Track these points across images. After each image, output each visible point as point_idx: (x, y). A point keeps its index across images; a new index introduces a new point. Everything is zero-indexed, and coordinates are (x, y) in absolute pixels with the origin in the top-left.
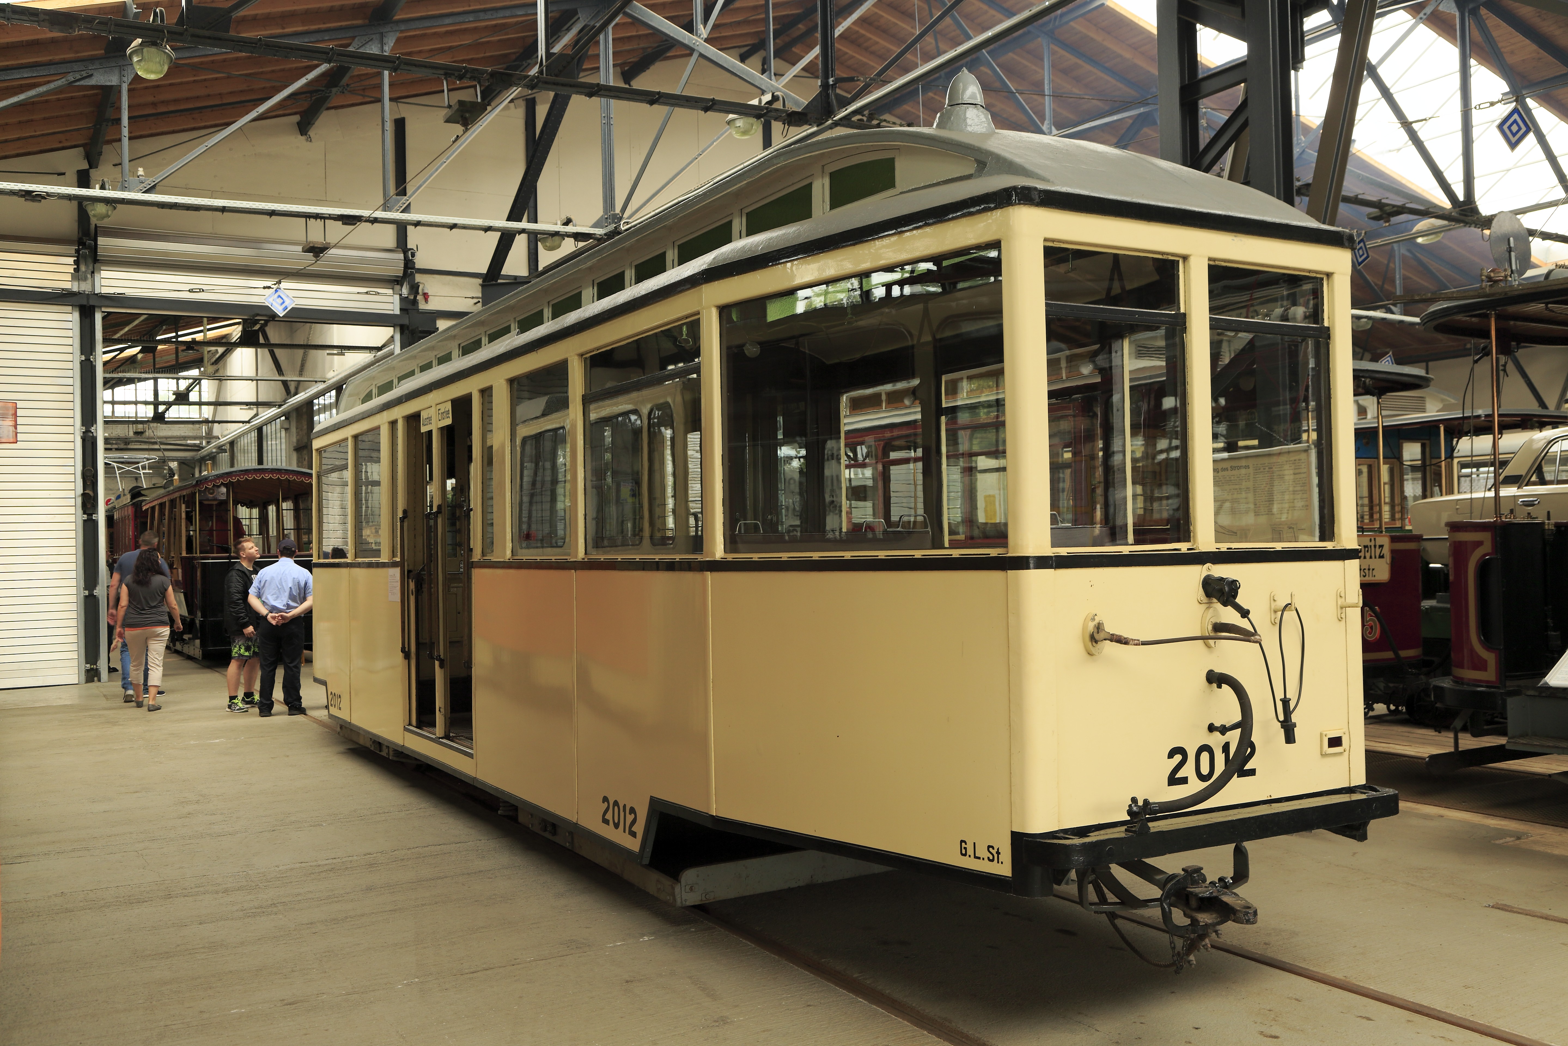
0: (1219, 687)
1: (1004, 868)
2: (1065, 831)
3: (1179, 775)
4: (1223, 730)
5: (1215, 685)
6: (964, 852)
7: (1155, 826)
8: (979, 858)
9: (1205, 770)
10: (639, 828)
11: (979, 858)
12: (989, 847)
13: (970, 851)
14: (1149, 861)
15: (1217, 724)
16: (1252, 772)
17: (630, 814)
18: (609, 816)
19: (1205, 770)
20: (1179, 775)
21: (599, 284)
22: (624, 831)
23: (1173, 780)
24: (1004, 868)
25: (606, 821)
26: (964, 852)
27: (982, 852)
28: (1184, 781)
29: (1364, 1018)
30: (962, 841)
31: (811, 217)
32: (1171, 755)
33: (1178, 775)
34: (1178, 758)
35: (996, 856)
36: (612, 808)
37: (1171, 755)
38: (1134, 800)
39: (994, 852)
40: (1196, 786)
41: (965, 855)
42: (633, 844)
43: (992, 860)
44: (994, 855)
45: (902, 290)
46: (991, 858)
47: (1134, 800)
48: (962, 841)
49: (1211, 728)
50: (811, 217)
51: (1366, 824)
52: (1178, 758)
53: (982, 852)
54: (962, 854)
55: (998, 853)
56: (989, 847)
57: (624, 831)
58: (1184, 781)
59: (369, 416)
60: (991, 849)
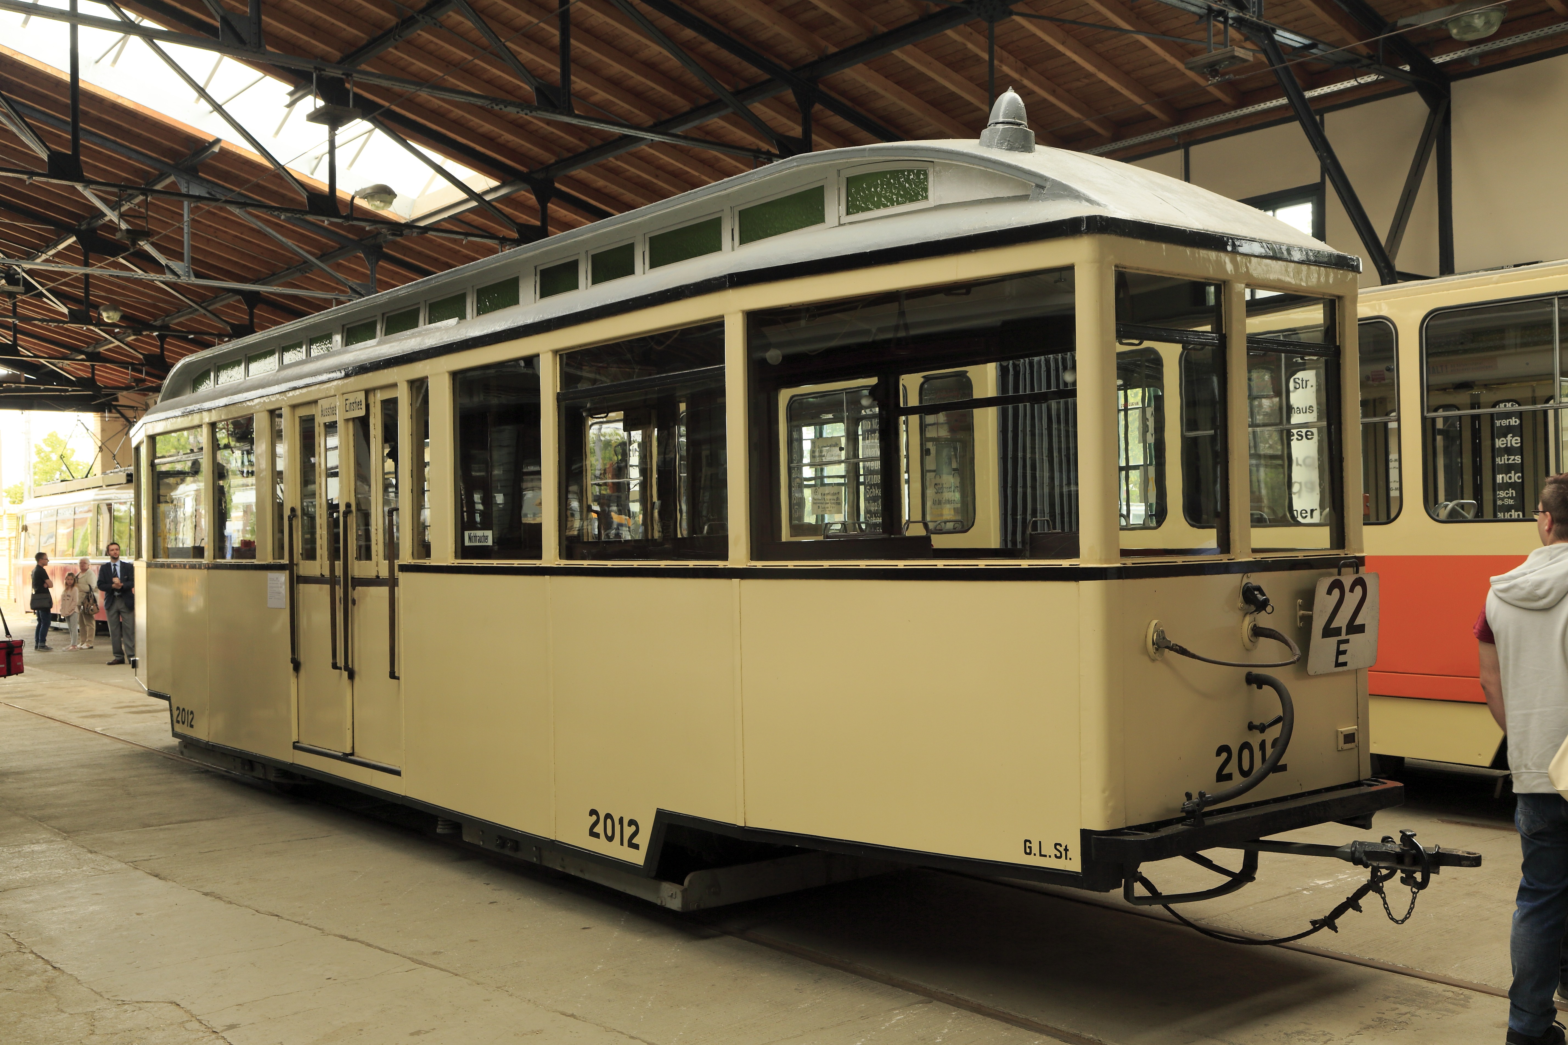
0: (1260, 687)
1: (1074, 864)
2: (1129, 828)
3: (1225, 772)
4: (1262, 728)
5: (1255, 686)
6: (1028, 850)
7: (1209, 821)
8: (1045, 856)
9: (1246, 767)
10: (644, 839)
11: (1045, 856)
12: (1056, 845)
13: (1036, 850)
14: (1201, 853)
15: (1257, 722)
16: (1284, 768)
17: (629, 825)
18: (599, 829)
19: (1246, 767)
20: (1225, 772)
21: (478, 290)
22: (622, 844)
23: (1222, 776)
24: (1074, 864)
25: (593, 834)
26: (1028, 850)
27: (1048, 849)
28: (1229, 777)
29: (409, 958)
30: (1026, 841)
31: (720, 249)
32: (1218, 753)
33: (1225, 772)
34: (1224, 755)
35: (1064, 853)
36: (600, 821)
37: (1218, 753)
38: (1189, 796)
39: (1062, 849)
40: (1238, 780)
41: (1030, 854)
42: (638, 858)
43: (1060, 857)
44: (1062, 851)
45: (596, 512)
46: (1058, 855)
47: (1189, 796)
48: (1026, 841)
49: (1251, 727)
50: (720, 249)
51: (1372, 815)
52: (1224, 755)
53: (1048, 849)
54: (1026, 853)
55: (1066, 850)
56: (1056, 845)
57: (622, 844)
58: (1229, 777)
59: (153, 524)
60: (1058, 847)
